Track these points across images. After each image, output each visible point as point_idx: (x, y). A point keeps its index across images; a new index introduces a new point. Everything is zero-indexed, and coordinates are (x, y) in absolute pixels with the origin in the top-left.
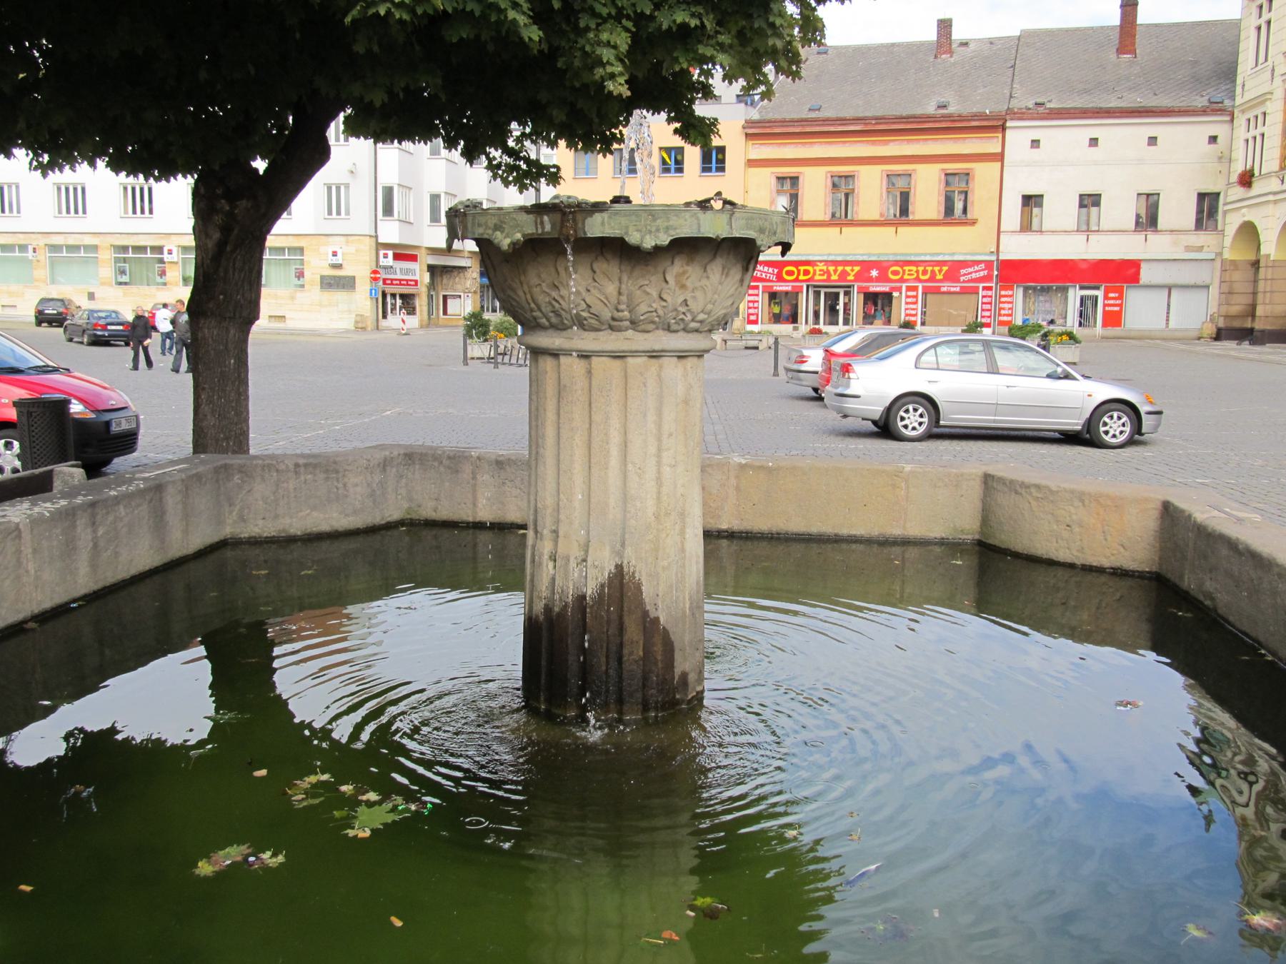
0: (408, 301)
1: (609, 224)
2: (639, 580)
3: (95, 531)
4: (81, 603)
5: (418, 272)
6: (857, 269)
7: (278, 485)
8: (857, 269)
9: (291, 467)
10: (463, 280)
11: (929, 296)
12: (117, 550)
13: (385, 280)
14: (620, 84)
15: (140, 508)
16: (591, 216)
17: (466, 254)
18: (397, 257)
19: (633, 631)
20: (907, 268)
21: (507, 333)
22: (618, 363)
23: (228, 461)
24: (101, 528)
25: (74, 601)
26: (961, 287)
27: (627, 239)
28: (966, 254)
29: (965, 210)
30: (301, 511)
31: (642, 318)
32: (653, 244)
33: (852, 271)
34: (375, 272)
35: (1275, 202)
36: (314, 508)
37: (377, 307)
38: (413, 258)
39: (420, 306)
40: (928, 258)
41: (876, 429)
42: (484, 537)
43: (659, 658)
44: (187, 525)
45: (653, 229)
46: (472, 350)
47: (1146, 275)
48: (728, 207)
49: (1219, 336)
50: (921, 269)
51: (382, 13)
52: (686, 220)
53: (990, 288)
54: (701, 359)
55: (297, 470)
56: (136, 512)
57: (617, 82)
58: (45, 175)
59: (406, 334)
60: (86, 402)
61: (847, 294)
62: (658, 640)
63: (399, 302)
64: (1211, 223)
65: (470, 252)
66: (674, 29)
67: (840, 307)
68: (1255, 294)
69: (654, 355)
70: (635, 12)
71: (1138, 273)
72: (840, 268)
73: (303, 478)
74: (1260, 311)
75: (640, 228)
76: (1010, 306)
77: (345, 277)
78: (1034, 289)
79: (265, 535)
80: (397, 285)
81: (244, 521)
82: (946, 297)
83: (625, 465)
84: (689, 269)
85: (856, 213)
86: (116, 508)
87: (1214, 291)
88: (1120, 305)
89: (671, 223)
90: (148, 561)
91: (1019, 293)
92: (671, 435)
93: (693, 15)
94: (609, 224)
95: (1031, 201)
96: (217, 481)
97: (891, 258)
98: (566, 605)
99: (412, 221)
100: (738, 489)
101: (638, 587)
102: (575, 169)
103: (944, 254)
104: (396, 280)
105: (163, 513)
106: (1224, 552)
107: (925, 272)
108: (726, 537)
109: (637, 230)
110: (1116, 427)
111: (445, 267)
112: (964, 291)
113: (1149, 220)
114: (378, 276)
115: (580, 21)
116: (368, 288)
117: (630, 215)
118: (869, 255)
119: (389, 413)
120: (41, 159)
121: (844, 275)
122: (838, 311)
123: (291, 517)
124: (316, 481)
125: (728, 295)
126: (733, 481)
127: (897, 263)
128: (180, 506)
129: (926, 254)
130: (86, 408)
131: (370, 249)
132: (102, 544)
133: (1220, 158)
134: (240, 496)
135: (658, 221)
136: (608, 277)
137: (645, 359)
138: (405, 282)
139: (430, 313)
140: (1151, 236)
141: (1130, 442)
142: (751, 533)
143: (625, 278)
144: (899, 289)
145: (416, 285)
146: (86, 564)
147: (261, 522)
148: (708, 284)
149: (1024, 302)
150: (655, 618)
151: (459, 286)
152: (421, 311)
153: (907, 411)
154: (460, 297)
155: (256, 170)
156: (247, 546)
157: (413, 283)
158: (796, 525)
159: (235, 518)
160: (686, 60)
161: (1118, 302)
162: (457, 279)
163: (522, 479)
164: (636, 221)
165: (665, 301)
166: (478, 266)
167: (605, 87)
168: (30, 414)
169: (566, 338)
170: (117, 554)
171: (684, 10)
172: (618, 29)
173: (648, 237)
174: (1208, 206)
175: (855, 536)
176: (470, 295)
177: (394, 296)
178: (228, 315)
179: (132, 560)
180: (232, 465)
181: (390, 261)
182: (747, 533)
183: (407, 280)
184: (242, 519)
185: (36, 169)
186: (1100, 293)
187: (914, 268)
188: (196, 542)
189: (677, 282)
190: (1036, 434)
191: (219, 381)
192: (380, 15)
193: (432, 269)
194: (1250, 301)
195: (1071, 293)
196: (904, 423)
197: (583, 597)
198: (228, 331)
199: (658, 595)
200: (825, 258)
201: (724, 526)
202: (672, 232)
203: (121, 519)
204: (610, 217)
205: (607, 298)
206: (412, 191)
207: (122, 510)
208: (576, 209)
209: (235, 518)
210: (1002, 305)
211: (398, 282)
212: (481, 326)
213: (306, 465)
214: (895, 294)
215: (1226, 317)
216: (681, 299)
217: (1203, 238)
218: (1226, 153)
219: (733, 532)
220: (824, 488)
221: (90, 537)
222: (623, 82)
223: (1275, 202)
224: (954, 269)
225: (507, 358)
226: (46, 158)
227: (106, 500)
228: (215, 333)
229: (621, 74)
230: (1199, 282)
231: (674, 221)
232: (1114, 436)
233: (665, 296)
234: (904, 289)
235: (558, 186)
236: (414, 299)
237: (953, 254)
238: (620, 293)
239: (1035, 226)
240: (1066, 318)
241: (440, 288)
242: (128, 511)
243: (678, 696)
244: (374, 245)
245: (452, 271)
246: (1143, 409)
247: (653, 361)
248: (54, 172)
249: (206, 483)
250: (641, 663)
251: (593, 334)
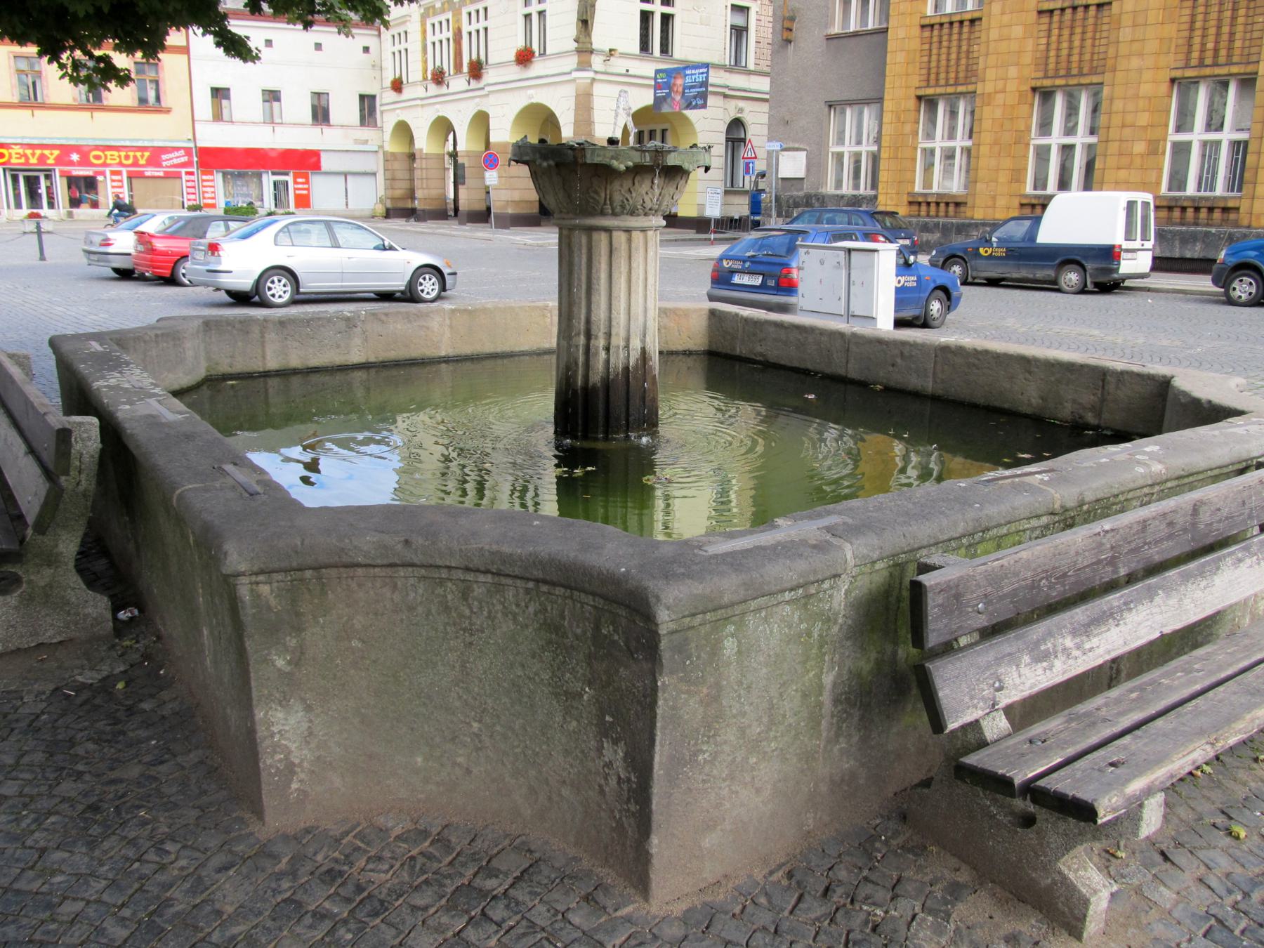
6: (56, 152)
8: (56, 152)
11: (134, 181)
20: (108, 153)
26: (165, 172)
28: (165, 141)
29: (158, 99)
33: (52, 156)
35: (422, 106)
40: (128, 144)
41: (232, 300)
42: (273, 383)
47: (326, 163)
49: (388, 214)
50: (123, 154)
53: (192, 173)
61: (48, 177)
64: (371, 120)
67: (43, 190)
68: (412, 180)
71: (319, 161)
72: (38, 152)
74: (419, 194)
76: (212, 189)
78: (232, 174)
82: (150, 182)
85: (47, 96)
87: (381, 177)
88: (308, 189)
91: (218, 177)
95: (219, 94)
97: (91, 143)
98: (618, 375)
100: (451, 327)
103: (144, 140)
106: (772, 329)
107: (127, 157)
108: (445, 362)
110: (429, 287)
112: (168, 176)
113: (321, 114)
118: (67, 139)
121: (42, 158)
122: (40, 195)
126: (448, 322)
127: (97, 148)
129: (124, 140)
133: (373, 66)
140: (326, 129)
141: (438, 298)
144: (103, 173)
149: (224, 187)
153: (273, 282)
158: (488, 348)
161: (306, 186)
174: (368, 104)
186: (290, 179)
187: (116, 153)
190: (348, 295)
194: (408, 186)
195: (265, 177)
196: (271, 292)
200: (19, 141)
201: (443, 354)
210: (205, 189)
213: (163, 335)
214: (100, 178)
215: (393, 199)
217: (367, 133)
218: (378, 63)
223: (422, 106)
224: (156, 155)
230: (368, 170)
232: (428, 293)
234: (108, 174)
237: (152, 140)
239: (226, 115)
240: (262, 200)
246: (446, 271)
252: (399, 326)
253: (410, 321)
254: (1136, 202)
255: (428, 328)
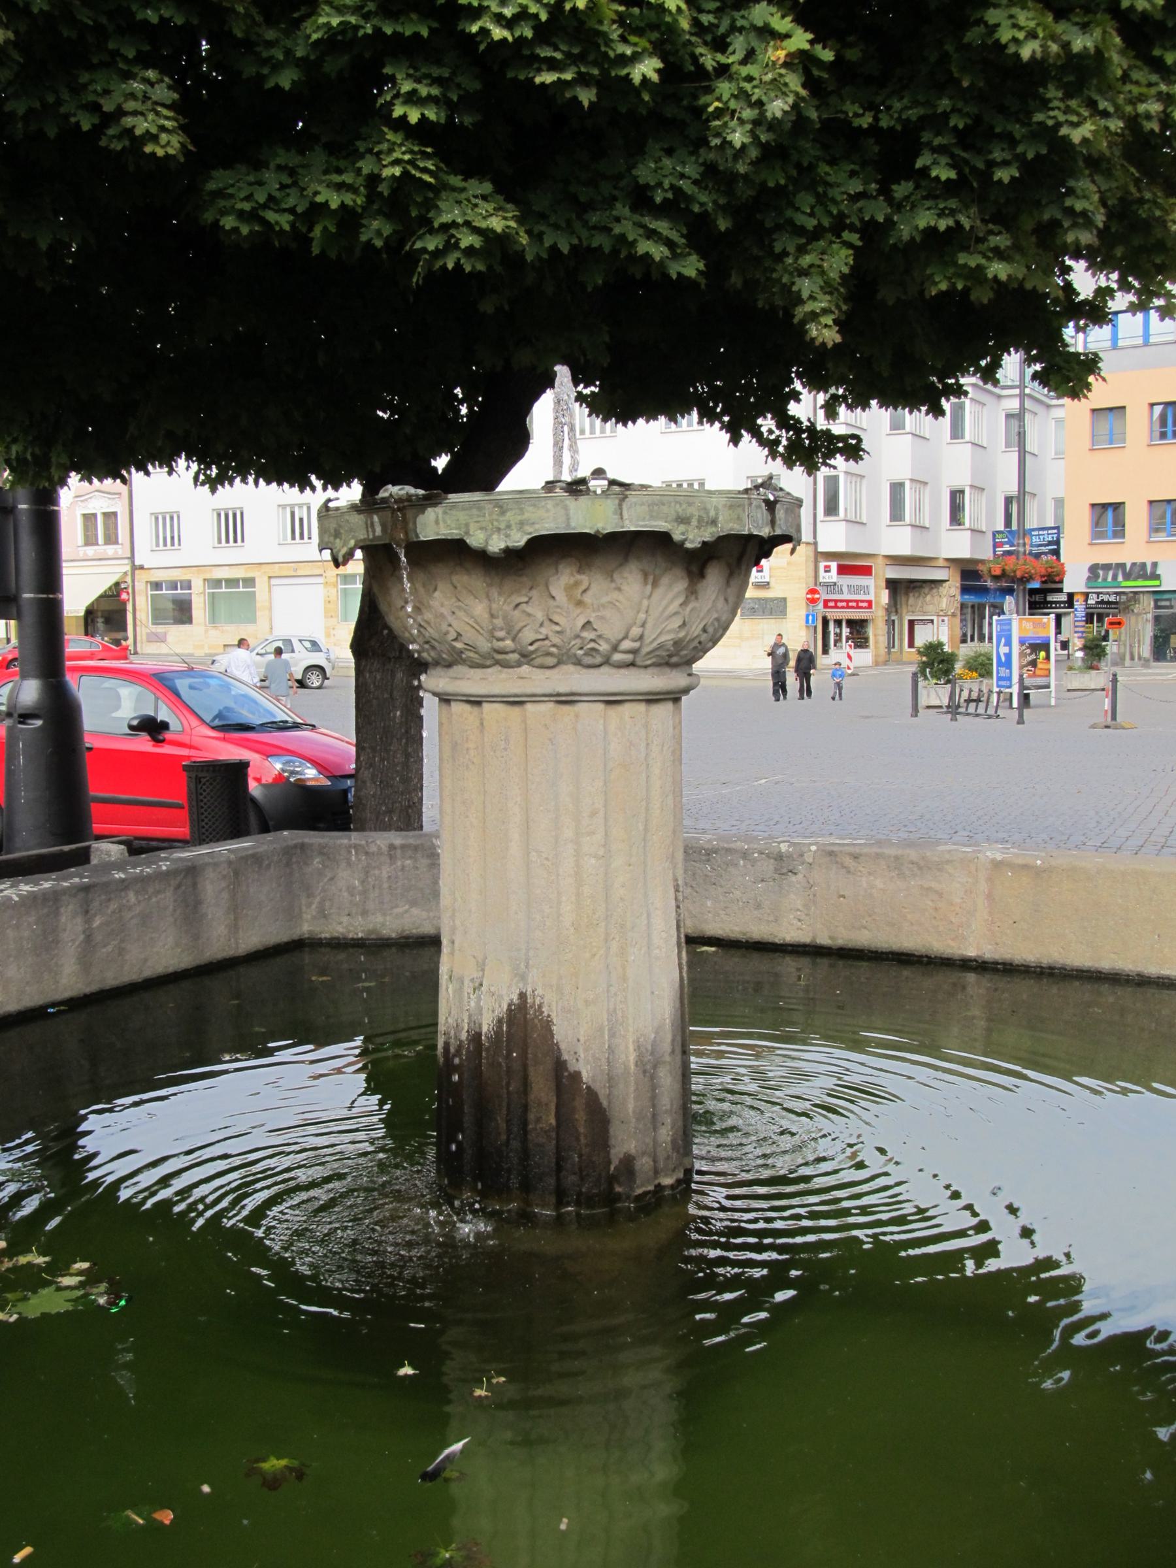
0: (858, 630)
1: (445, 522)
2: (549, 1016)
3: (88, 921)
4: (62, 1008)
5: (874, 590)
7: (367, 873)
9: (385, 849)
10: (936, 598)
12: (123, 945)
13: (826, 602)
14: (826, 326)
15: (161, 896)
16: (423, 513)
17: (941, 563)
18: (843, 570)
19: (542, 1090)
21: (983, 671)
22: (516, 710)
23: (306, 840)
24: (97, 918)
25: (53, 1005)
27: (468, 541)
30: (397, 906)
31: (531, 648)
32: (503, 546)
34: (813, 591)
36: (414, 903)
37: (815, 638)
38: (866, 571)
39: (875, 635)
43: (582, 1130)
44: (236, 919)
45: (502, 526)
46: (928, 695)
48: (616, 488)
51: (450, 266)
52: (548, 511)
54: (444, 706)
55: (392, 853)
56: (154, 900)
57: (820, 323)
58: (213, 490)
59: (853, 675)
60: (325, 768)
62: (579, 1103)
63: (846, 631)
65: (947, 560)
66: (918, 239)
69: (566, 700)
70: (862, 220)
73: (399, 863)
75: (484, 524)
77: (772, 600)
79: (351, 936)
80: (843, 607)
81: (325, 917)
83: (528, 854)
84: (584, 579)
86: (123, 894)
89: (526, 515)
90: (172, 962)
92: (594, 814)
93: (941, 215)
94: (445, 522)
96: (288, 864)
99: (864, 520)
100: (990, 897)
101: (547, 1025)
102: (1093, 436)
104: (842, 601)
105: (198, 903)
109: (481, 529)
111: (912, 582)
114: (817, 596)
115: (775, 244)
116: (803, 613)
117: (471, 508)
119: (764, 781)
120: (208, 472)
123: (384, 915)
124: (417, 868)
125: (667, 613)
126: (983, 886)
128: (225, 895)
130: (320, 773)
131: (806, 561)
132: (98, 937)
134: (321, 884)
135: (509, 514)
136: (473, 594)
137: (551, 705)
138: (854, 604)
139: (891, 645)
142: (1011, 964)
143: (495, 595)
145: (870, 606)
146: (73, 961)
147: (345, 919)
148: (621, 598)
150: (575, 1072)
151: (930, 608)
152: (876, 642)
154: (932, 621)
155: (435, 469)
156: (328, 950)
157: (865, 604)
158: (1078, 957)
159: (314, 913)
160: (945, 277)
162: (928, 598)
163: (694, 874)
164: (478, 516)
165: (557, 624)
166: (959, 579)
167: (806, 332)
168: (198, 780)
169: (452, 678)
170: (121, 951)
171: (929, 209)
172: (834, 246)
173: (495, 537)
175: (1168, 978)
176: (946, 619)
177: (838, 623)
178: (392, 655)
179: (146, 960)
180: (312, 845)
181: (833, 576)
182: (1004, 964)
183: (857, 601)
184: (323, 914)
185: (203, 484)
188: (251, 939)
189: (570, 597)
191: (381, 738)
192: (447, 269)
193: (894, 586)
197: (478, 1035)
198: (393, 676)
199: (578, 1040)
201: (971, 953)
202: (529, 529)
203: (130, 908)
204: (445, 513)
205: (477, 623)
206: (865, 481)
207: (132, 897)
208: (406, 504)
209: (314, 913)
211: (844, 604)
212: (941, 662)
216: (581, 622)
219: (984, 962)
220: (1120, 901)
221: (80, 928)
222: (830, 322)
225: (982, 705)
226: (214, 471)
227: (106, 885)
228: (378, 677)
229: (825, 311)
231: (530, 513)
233: (556, 618)
235: (860, 462)
236: (867, 627)
238: (492, 616)
241: (904, 611)
242: (140, 898)
243: (618, 1189)
244: (812, 554)
245: (921, 587)
247: (566, 708)
248: (223, 485)
249: (269, 866)
250: (554, 1135)
251: (479, 672)
252: (879, 883)
253: (901, 875)
254: (254, 587)
255: (940, 895)
